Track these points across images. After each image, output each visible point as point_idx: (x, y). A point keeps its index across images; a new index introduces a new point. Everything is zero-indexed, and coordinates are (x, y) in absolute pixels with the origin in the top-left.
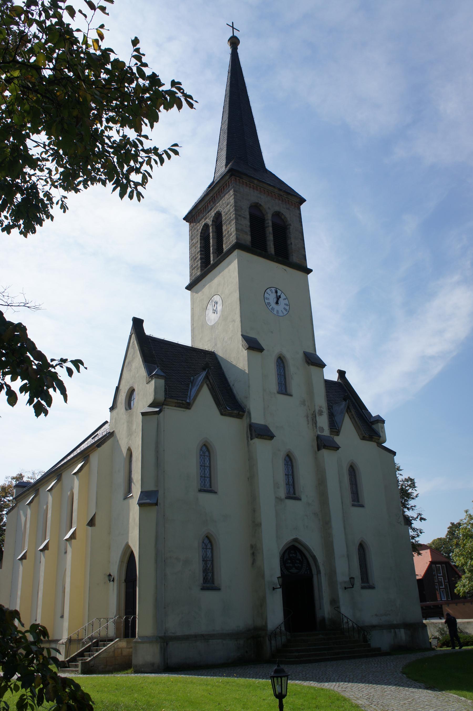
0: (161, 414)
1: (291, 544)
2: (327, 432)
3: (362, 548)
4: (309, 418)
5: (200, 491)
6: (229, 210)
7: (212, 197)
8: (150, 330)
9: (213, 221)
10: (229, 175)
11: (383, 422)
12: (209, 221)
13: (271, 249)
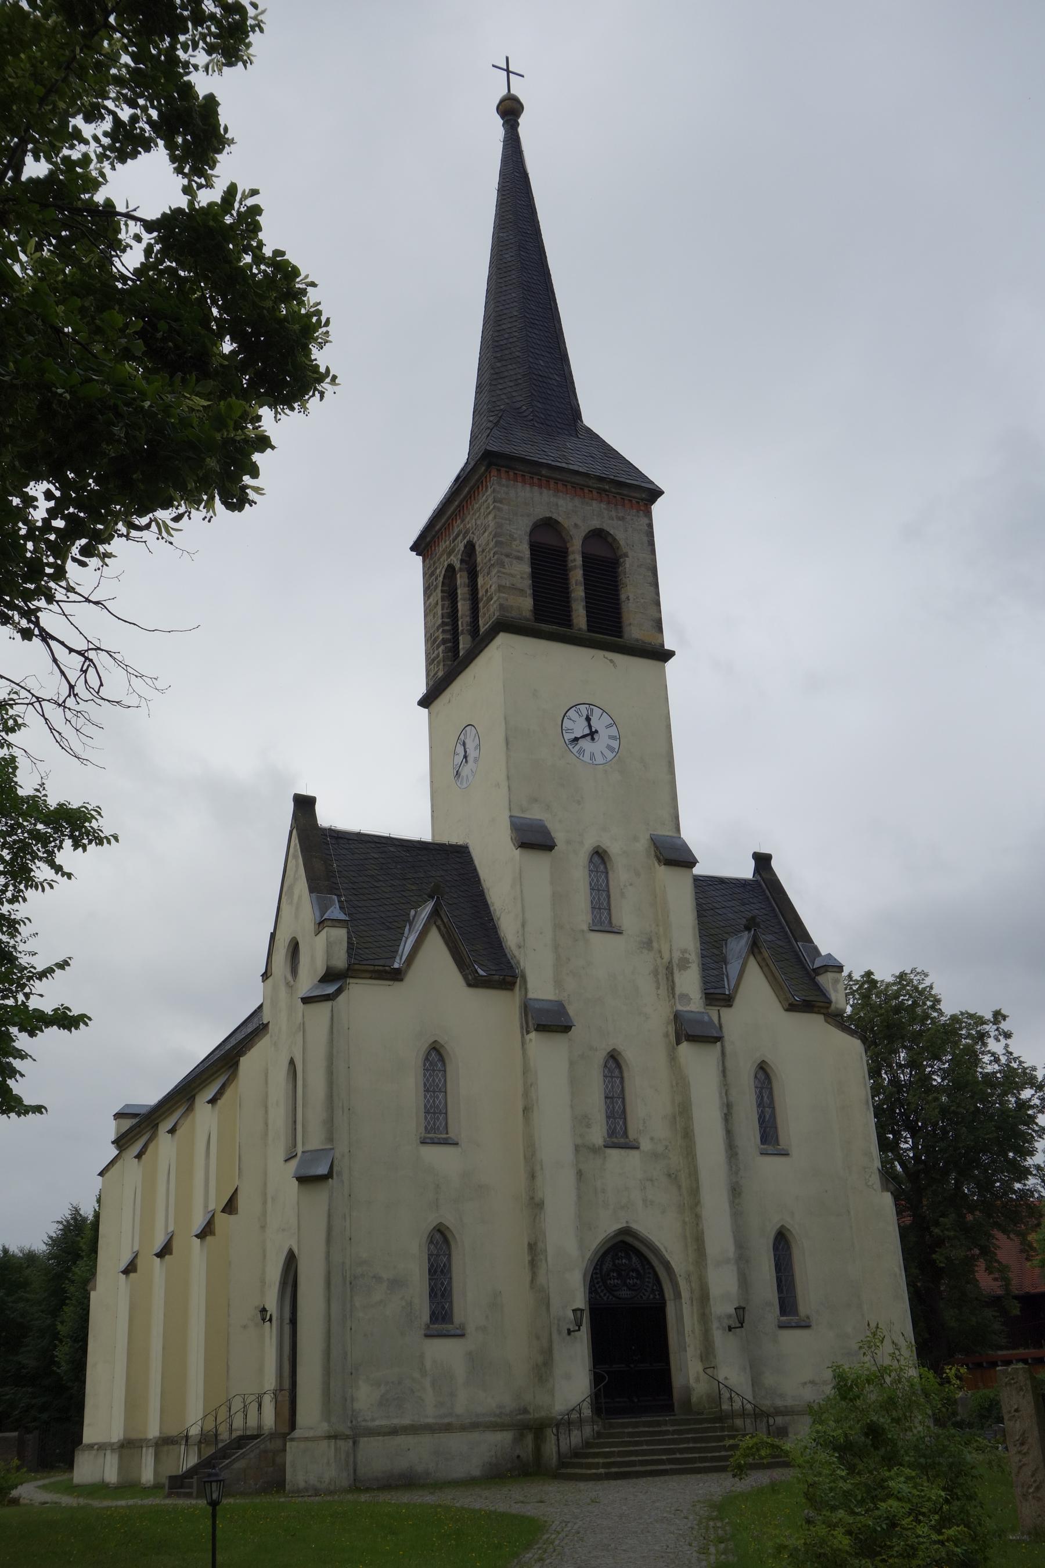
0: (341, 998)
2: (695, 1003)
3: (782, 1242)
4: (660, 977)
8: (327, 816)
12: (455, 560)
13: (580, 617)
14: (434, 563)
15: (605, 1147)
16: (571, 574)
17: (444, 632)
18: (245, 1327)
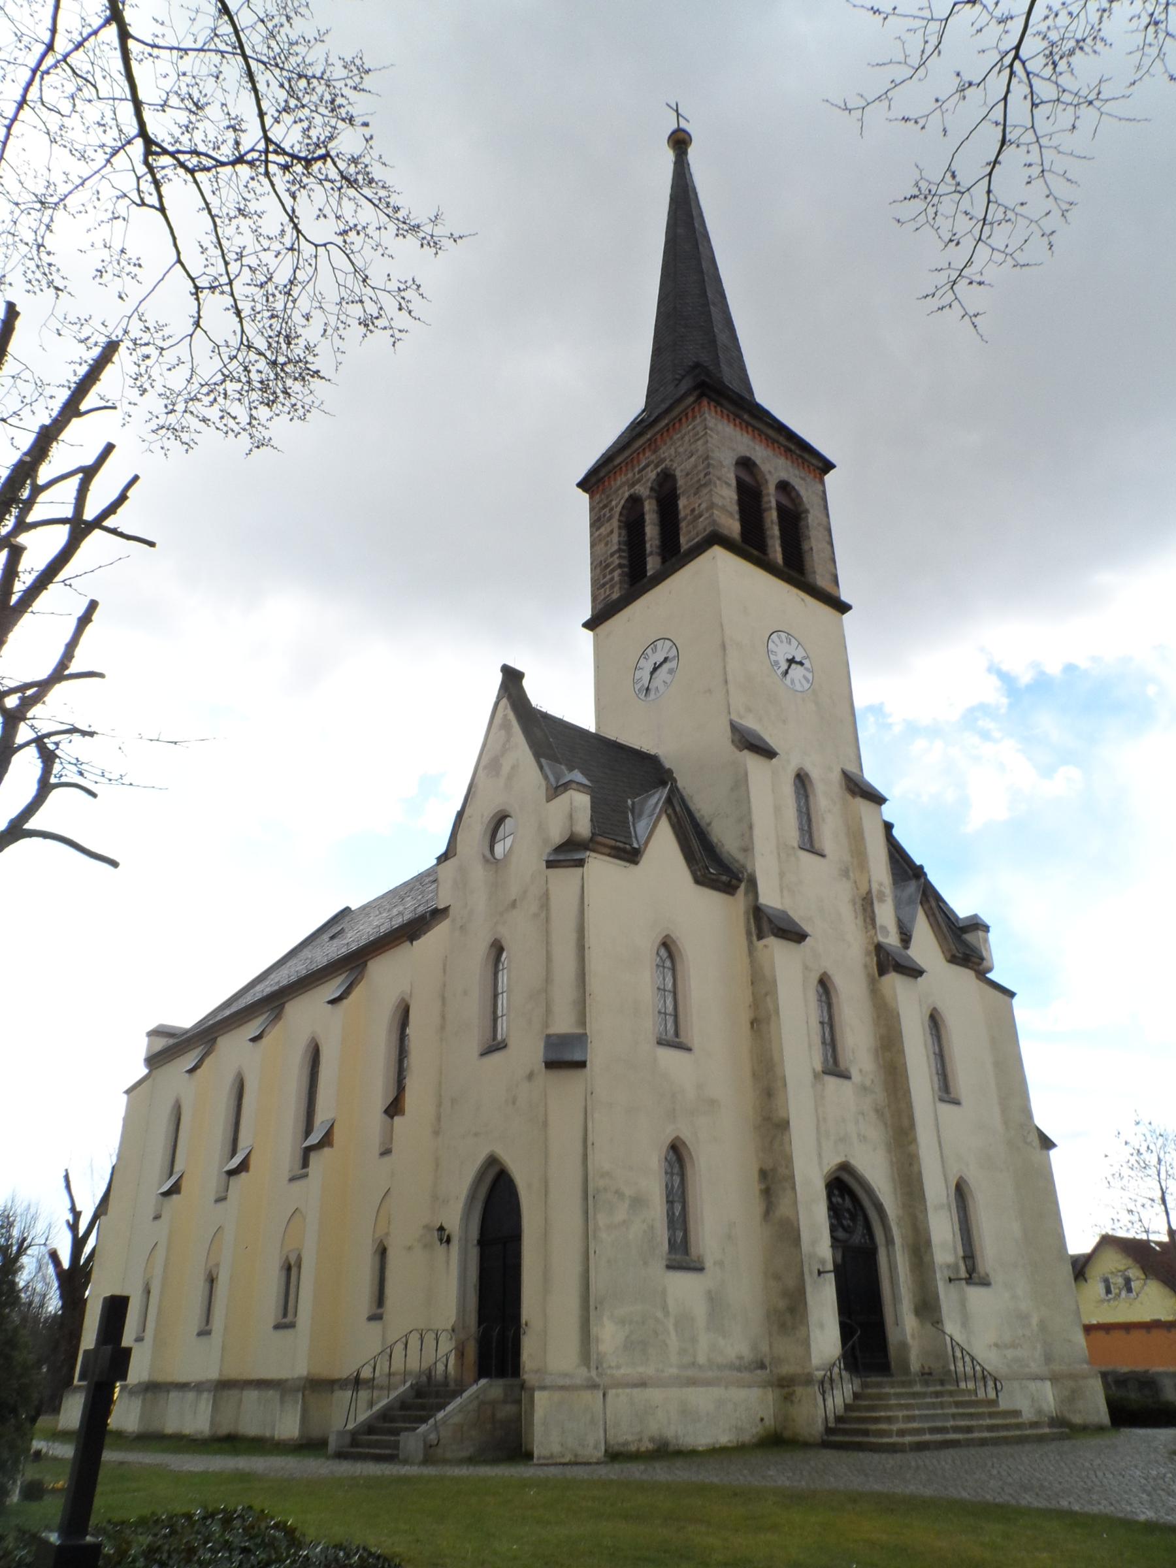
1: (834, 1176)
2: (892, 939)
5: (660, 1043)
6: (695, 466)
7: (649, 440)
9: (652, 489)
10: (696, 394)
11: (986, 928)
13: (777, 553)
14: (608, 497)
15: (824, 1072)
16: (766, 514)
17: (620, 557)
18: (410, 1248)
